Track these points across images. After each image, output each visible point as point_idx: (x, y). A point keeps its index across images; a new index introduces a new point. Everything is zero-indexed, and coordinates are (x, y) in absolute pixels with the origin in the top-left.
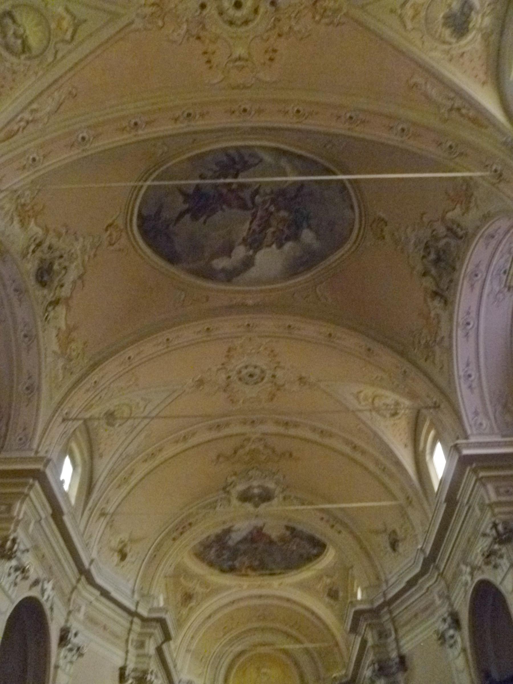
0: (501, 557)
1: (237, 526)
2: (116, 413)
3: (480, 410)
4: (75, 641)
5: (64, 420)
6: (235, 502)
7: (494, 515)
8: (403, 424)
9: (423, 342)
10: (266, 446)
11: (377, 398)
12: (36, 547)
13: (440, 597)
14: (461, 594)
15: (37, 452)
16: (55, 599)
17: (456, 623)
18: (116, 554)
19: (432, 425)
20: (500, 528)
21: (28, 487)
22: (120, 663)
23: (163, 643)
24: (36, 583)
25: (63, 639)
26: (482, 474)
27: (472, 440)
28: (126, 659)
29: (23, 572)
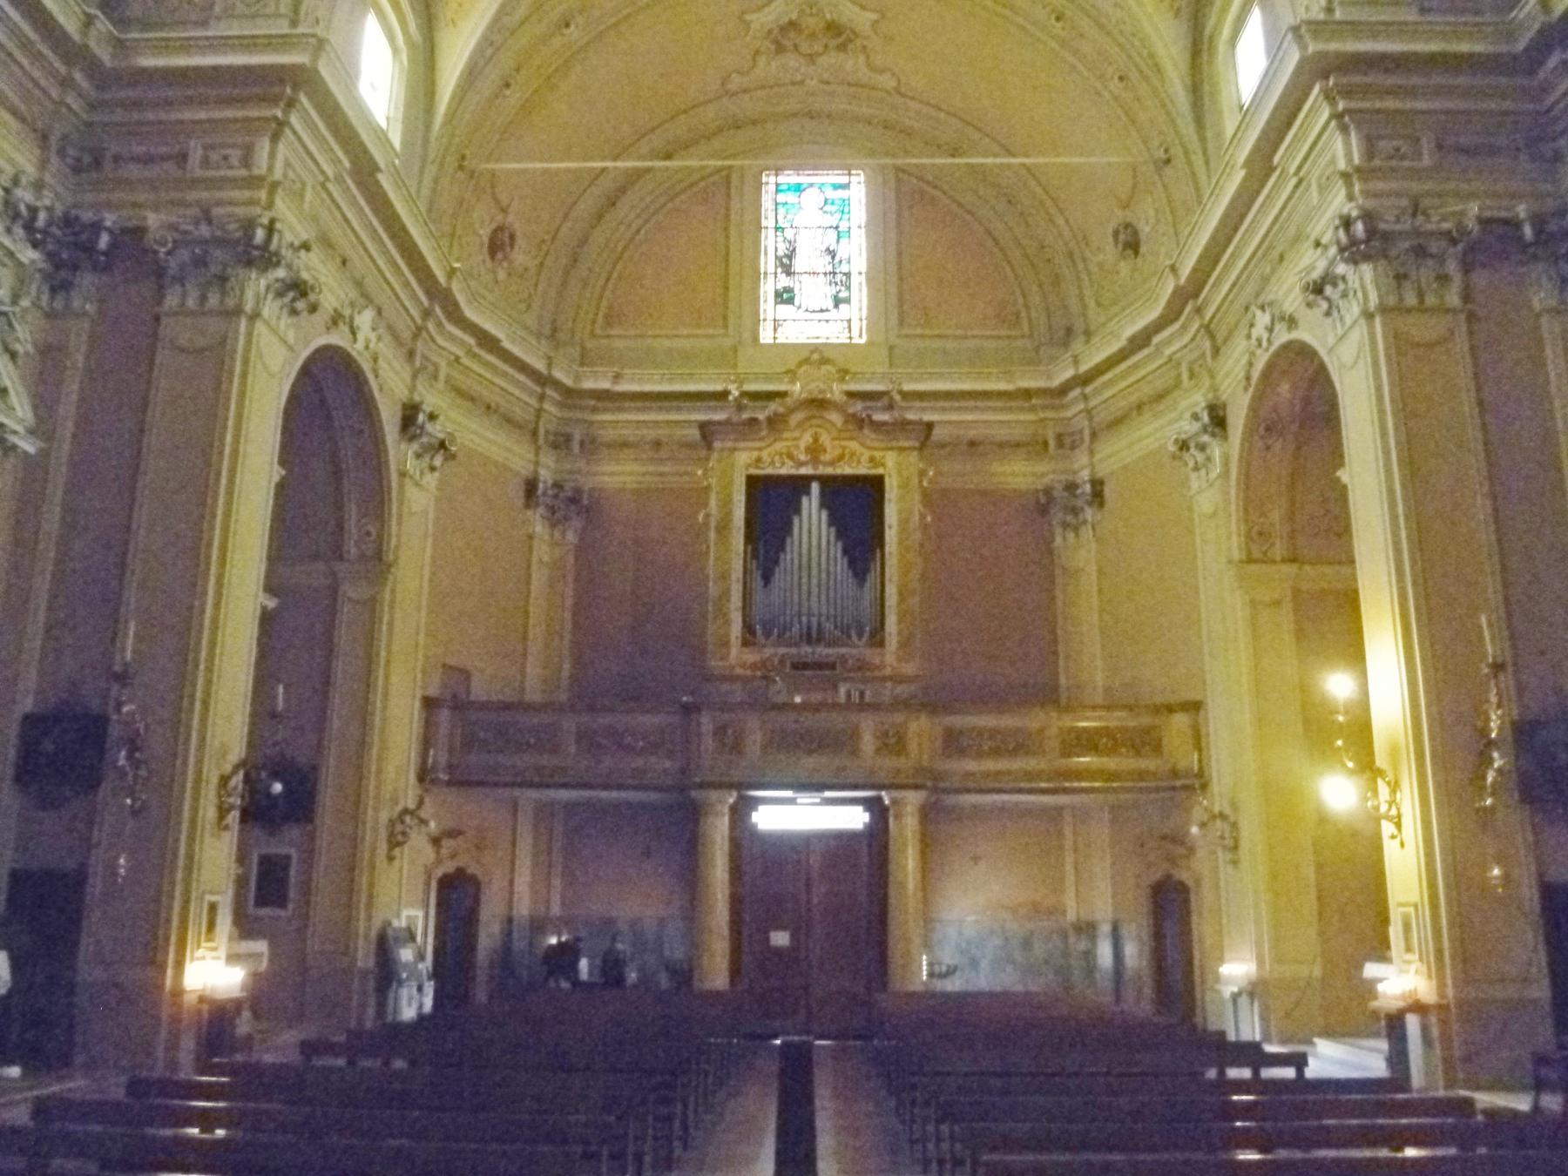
4: (436, 430)
12: (327, 242)
14: (1237, 370)
17: (1218, 420)
20: (1359, 228)
21: (282, 104)
24: (336, 319)
25: (409, 418)
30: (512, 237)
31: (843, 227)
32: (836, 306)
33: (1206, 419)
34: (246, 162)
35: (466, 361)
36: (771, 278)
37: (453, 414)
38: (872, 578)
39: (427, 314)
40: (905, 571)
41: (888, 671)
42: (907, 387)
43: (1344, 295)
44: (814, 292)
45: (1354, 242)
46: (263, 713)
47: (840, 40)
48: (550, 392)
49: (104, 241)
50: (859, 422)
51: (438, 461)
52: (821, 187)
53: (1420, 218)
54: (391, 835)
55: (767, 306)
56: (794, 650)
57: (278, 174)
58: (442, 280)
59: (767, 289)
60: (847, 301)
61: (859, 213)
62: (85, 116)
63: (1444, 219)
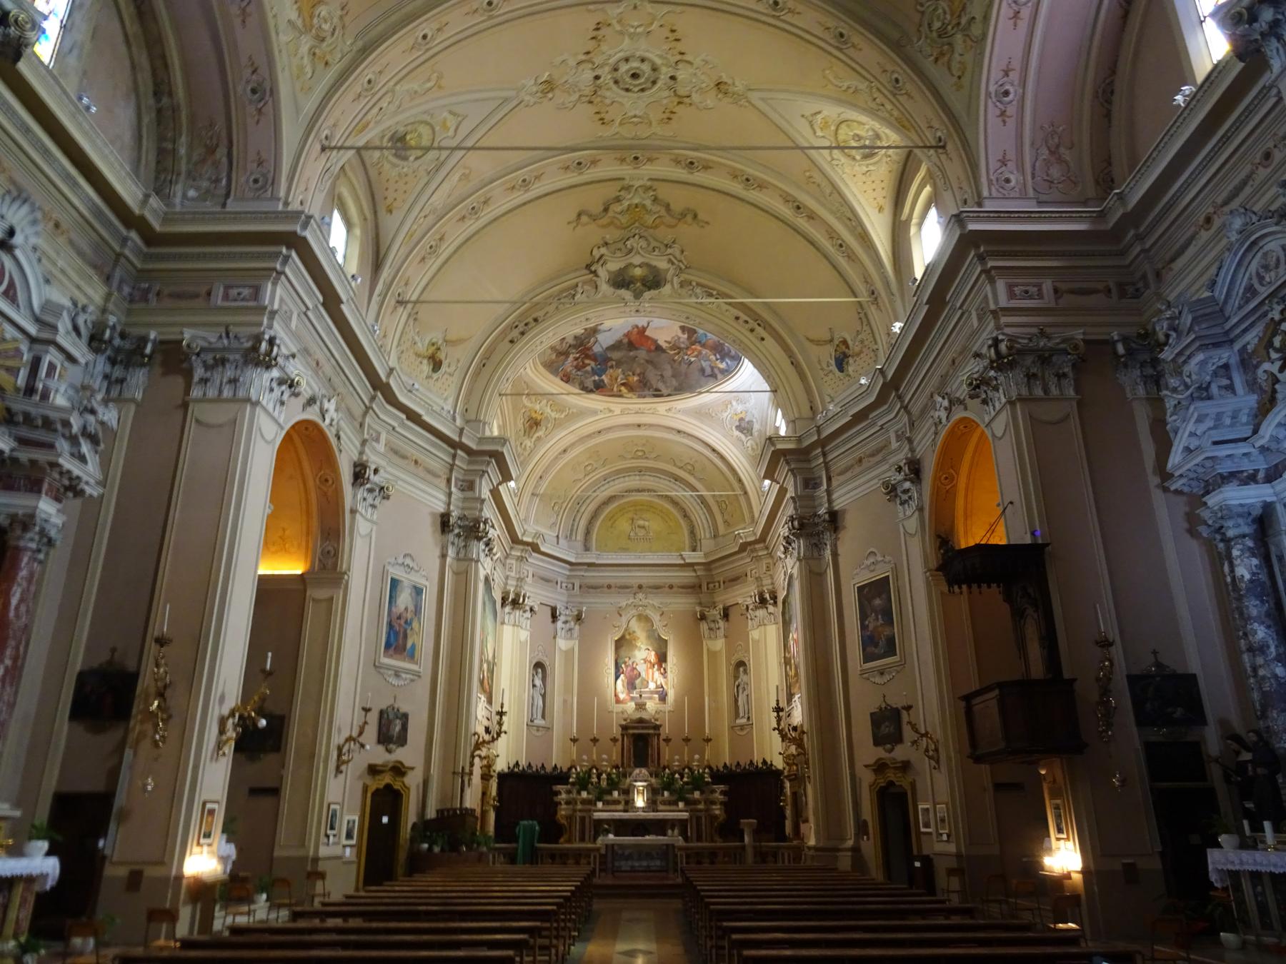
0: (996, 389)
1: (607, 324)
2: (408, 137)
3: (1011, 155)
5: (323, 149)
6: (605, 288)
7: (998, 327)
8: (883, 169)
9: (937, 25)
10: (655, 200)
11: (843, 126)
12: (306, 351)
13: (898, 438)
15: (286, 204)
16: (342, 424)
17: (915, 470)
18: (425, 361)
19: (930, 176)
20: (1003, 347)
22: (441, 508)
23: (500, 484)
24: (311, 401)
25: (360, 474)
26: (990, 264)
27: (989, 206)
28: (449, 504)
29: (290, 386)
46: (254, 671)
48: (459, 452)
49: (148, 350)
57: (276, 307)
62: (139, 266)
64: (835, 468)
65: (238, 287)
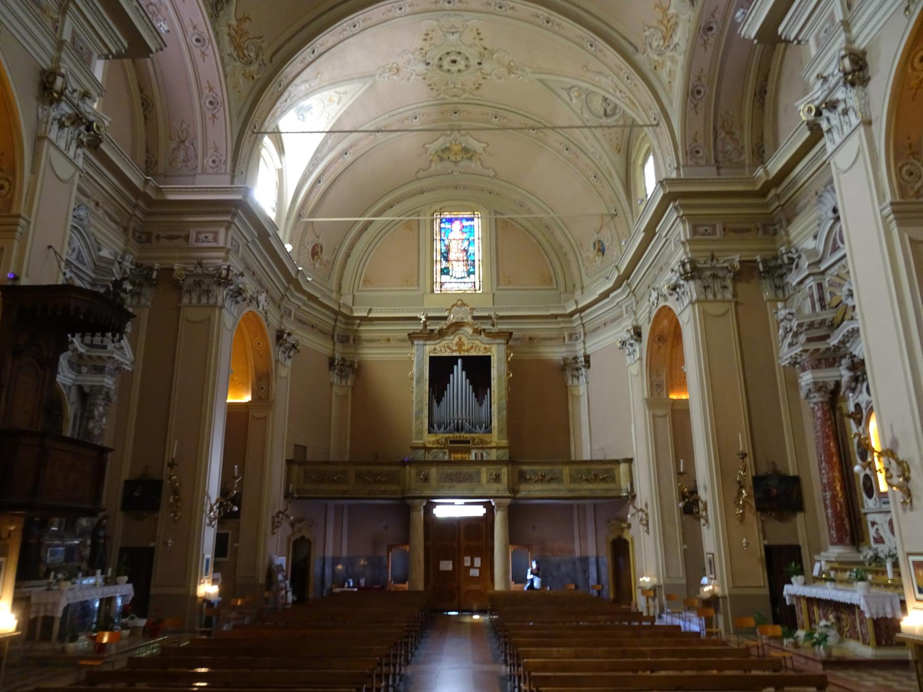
4: (291, 340)
12: (248, 268)
17: (638, 333)
20: (688, 267)
30: (322, 248)
31: (472, 238)
32: (469, 276)
33: (632, 332)
34: (215, 239)
35: (303, 307)
36: (438, 264)
37: (298, 332)
38: (486, 403)
39: (287, 289)
40: (500, 400)
41: (494, 445)
42: (501, 314)
43: (683, 293)
44: (458, 269)
45: (686, 272)
47: (469, 155)
48: (339, 318)
49: (155, 275)
50: (478, 332)
51: (292, 354)
52: (461, 219)
53: (715, 262)
54: (273, 523)
55: (438, 278)
56: (451, 435)
57: (229, 246)
58: (293, 274)
59: (438, 268)
60: (474, 273)
61: (478, 233)
62: (143, 219)
63: (724, 262)
64: (589, 327)
65: (205, 232)
